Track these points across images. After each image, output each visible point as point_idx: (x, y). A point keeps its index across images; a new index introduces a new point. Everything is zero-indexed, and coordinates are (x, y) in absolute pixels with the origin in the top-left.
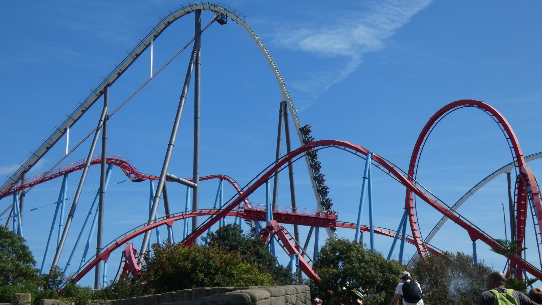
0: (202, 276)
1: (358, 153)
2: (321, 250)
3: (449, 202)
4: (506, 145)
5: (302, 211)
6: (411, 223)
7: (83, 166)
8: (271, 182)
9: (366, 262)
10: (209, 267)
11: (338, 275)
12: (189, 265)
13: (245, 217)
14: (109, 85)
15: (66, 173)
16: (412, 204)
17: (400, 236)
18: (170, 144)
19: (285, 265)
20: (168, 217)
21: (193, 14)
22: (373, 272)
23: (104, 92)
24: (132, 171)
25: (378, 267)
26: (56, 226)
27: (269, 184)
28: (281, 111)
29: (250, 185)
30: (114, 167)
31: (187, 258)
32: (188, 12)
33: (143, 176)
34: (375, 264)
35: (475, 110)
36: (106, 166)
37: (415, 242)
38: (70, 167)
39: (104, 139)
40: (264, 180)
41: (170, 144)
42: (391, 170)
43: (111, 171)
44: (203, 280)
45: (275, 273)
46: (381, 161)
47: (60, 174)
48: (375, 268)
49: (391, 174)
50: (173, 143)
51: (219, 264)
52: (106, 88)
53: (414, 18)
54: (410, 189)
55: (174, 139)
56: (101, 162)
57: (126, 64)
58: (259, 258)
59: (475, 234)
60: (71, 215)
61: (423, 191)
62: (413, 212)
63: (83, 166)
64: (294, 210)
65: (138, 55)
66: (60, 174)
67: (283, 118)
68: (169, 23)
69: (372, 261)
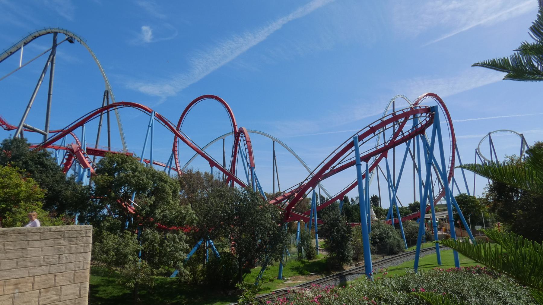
3: (200, 145)
9: (140, 172)
16: (177, 144)
18: (28, 107)
21: (52, 35)
22: (145, 180)
25: (149, 176)
27: (84, 127)
28: (104, 95)
32: (49, 33)
33: (13, 127)
34: (147, 174)
37: (177, 170)
41: (28, 107)
42: (166, 123)
46: (160, 118)
48: (147, 178)
50: (30, 106)
54: (177, 135)
55: (31, 103)
59: (213, 164)
61: (185, 137)
62: (177, 153)
65: (12, 53)
67: (106, 99)
68: (36, 37)
69: (145, 171)
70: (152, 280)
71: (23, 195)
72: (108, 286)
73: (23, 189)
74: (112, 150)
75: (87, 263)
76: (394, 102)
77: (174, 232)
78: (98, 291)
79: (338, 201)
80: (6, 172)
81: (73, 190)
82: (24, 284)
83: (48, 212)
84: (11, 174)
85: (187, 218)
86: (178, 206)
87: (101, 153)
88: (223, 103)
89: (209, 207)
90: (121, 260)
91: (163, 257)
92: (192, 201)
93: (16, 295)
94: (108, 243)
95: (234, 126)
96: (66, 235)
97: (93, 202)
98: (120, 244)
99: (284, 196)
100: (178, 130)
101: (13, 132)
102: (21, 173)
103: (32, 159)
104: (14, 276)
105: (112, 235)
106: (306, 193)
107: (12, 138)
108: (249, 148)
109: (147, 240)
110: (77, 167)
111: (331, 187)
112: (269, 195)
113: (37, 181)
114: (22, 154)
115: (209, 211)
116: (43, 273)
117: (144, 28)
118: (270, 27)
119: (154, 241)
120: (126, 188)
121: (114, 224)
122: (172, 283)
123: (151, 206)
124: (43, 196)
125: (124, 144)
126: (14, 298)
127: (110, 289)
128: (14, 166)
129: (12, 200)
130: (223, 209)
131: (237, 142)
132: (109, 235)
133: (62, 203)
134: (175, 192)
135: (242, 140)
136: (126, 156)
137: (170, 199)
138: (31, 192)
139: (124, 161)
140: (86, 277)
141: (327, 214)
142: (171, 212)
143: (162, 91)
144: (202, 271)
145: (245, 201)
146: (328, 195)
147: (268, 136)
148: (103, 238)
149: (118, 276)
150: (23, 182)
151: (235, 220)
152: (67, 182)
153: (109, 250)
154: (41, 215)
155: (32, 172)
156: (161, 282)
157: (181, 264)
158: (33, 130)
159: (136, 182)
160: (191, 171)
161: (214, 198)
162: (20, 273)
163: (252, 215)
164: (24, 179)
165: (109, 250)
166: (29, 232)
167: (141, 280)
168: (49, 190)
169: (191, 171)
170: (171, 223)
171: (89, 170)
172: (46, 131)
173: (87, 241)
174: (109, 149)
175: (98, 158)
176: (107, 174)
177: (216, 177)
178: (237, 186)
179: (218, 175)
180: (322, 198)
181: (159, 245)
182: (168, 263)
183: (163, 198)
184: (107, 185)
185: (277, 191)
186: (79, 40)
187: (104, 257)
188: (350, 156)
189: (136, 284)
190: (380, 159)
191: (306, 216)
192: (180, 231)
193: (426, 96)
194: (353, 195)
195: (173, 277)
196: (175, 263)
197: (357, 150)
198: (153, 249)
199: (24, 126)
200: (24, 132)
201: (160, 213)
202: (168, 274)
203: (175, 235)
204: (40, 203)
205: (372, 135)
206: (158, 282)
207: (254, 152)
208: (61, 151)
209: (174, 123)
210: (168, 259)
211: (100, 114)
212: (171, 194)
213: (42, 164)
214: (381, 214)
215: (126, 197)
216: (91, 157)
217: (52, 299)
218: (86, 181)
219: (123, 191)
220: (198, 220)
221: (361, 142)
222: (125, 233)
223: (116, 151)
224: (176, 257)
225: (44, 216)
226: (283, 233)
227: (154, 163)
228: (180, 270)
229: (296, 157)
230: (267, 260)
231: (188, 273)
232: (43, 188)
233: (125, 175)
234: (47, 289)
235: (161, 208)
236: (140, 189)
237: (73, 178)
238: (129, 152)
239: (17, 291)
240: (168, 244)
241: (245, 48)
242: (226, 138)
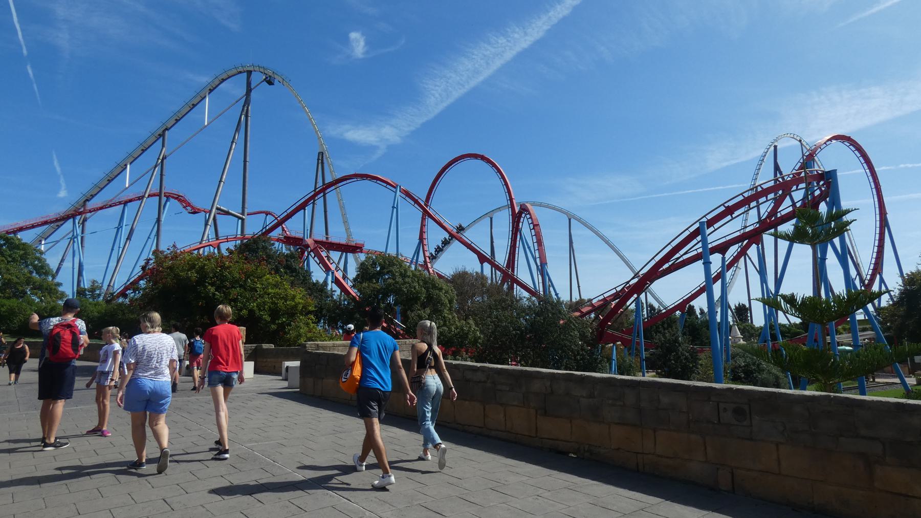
0: (212, 289)
4: (502, 190)
5: (333, 239)
6: (424, 251)
7: (141, 198)
8: (308, 209)
10: (223, 279)
11: (379, 291)
12: (193, 275)
13: (283, 242)
14: (167, 129)
15: (126, 203)
18: (220, 181)
19: (321, 281)
20: (217, 239)
23: (162, 135)
24: (189, 204)
26: (116, 247)
30: (172, 200)
31: (192, 267)
32: (241, 72)
35: (479, 162)
36: (164, 199)
38: (129, 198)
39: (162, 175)
40: (302, 207)
41: (220, 181)
43: (168, 203)
44: (214, 294)
45: (310, 289)
46: (407, 194)
51: (238, 276)
52: (164, 131)
54: (426, 214)
56: (159, 195)
57: (149, 143)
58: (292, 272)
59: (482, 259)
60: (129, 238)
62: (425, 242)
63: (141, 198)
64: (327, 238)
65: (194, 106)
66: (120, 203)
74: (330, 240)
76: (775, 147)
79: (678, 313)
88: (494, 165)
95: (511, 199)
99: (592, 305)
106: (628, 303)
111: (668, 292)
117: (354, 35)
118: (551, 14)
125: (347, 229)
141: (660, 332)
146: (660, 303)
158: (227, 213)
172: (243, 214)
178: (518, 291)
180: (651, 307)
188: (695, 247)
190: (748, 246)
191: (626, 337)
193: (830, 140)
194: (700, 303)
197: (704, 241)
199: (217, 209)
200: (218, 216)
205: (729, 217)
207: (546, 242)
209: (422, 196)
214: (752, 335)
221: (712, 229)
229: (602, 238)
238: (359, 242)
241: (509, 55)
242: (496, 216)
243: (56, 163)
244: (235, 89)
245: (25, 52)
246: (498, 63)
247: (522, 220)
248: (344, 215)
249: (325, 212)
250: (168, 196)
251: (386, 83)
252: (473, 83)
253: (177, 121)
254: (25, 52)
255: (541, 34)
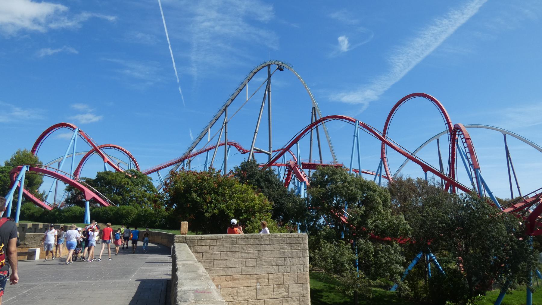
0: (195, 195)
1: (350, 122)
2: (313, 175)
3: (410, 150)
7: (215, 147)
9: (349, 183)
17: (378, 174)
21: (267, 68)
23: (225, 110)
24: (241, 148)
25: (358, 186)
29: (287, 146)
30: (232, 146)
32: (264, 66)
34: (356, 184)
36: (227, 146)
37: (387, 178)
39: (225, 132)
41: (255, 132)
42: (371, 131)
46: (365, 126)
47: (205, 151)
49: (371, 133)
52: (226, 107)
53: (393, 86)
54: (384, 142)
56: (225, 144)
59: (426, 168)
61: (392, 143)
62: (386, 160)
63: (215, 147)
65: (241, 90)
66: (205, 151)
67: (314, 116)
68: (255, 73)
69: (353, 181)
70: (370, 290)
71: (257, 207)
72: (330, 292)
73: (257, 202)
74: (324, 163)
75: (306, 267)
77: (389, 243)
78: (322, 296)
80: (245, 189)
81: (293, 202)
82: (263, 280)
83: (276, 222)
84: (248, 190)
85: (401, 229)
86: (389, 216)
87: (314, 166)
88: (433, 99)
89: (425, 217)
90: (339, 268)
91: (379, 268)
92: (404, 210)
93: (258, 287)
94: (325, 251)
95: (449, 123)
96: (288, 241)
97: (310, 212)
98: (336, 253)
99: (525, 201)
100: (384, 136)
101: (246, 155)
102: (254, 189)
103: (262, 177)
104: (255, 272)
105: (329, 244)
107: (246, 161)
108: (470, 147)
109: (361, 250)
110: (296, 181)
112: (505, 201)
113: (266, 196)
114: (254, 174)
115: (425, 221)
116: (275, 272)
117: (340, 39)
119: (368, 251)
120: (338, 199)
121: (329, 233)
122: (392, 296)
123: (362, 216)
124: (271, 208)
125: (334, 156)
126: (257, 289)
127: (332, 295)
128: (249, 184)
129: (250, 212)
130: (441, 218)
131: (453, 141)
132: (326, 243)
133: (287, 213)
134: (385, 201)
135: (459, 138)
136: (335, 168)
137: (381, 208)
138: (262, 204)
139: (334, 173)
140: (306, 279)
142: (383, 223)
143: (363, 98)
144: (425, 288)
145: (467, 210)
147: (496, 129)
148: (321, 246)
149: (338, 284)
150: (256, 197)
151: (458, 232)
152: (288, 195)
153: (327, 258)
154: (271, 224)
155: (262, 188)
156: (379, 294)
157: (398, 277)
158: (261, 152)
159: (346, 192)
160: (401, 178)
161: (429, 206)
162: (259, 270)
163: (479, 225)
164: (257, 194)
165: (327, 258)
166: (262, 238)
167: (359, 290)
168: (275, 203)
169: (401, 178)
170: (383, 233)
171: (305, 183)
172: (270, 151)
173: (304, 247)
174: (321, 162)
175: (313, 171)
176: (319, 186)
177: (430, 183)
179: (435, 180)
181: (373, 256)
182: (384, 275)
183: (373, 208)
184: (321, 197)
185: (516, 195)
186: (287, 67)
187: (323, 264)
189: (355, 293)
192: (394, 242)
195: (393, 290)
196: (392, 276)
198: (368, 259)
199: (254, 149)
200: (254, 154)
201: (372, 223)
202: (387, 287)
203: (389, 246)
204: (269, 214)
206: (377, 294)
207: (476, 149)
208: (283, 168)
209: (379, 129)
210: (384, 270)
211: (309, 130)
212: (381, 203)
213: (268, 180)
215: (338, 208)
216: (306, 171)
217: (283, 294)
218: (304, 194)
219: (335, 202)
220: (413, 231)
222: (340, 242)
223: (327, 163)
224: (392, 270)
225: (274, 225)
226: (526, 250)
227: (363, 172)
228: (398, 284)
230: (507, 282)
231: (407, 287)
232: (271, 201)
233: (335, 186)
234: (279, 286)
235: (372, 218)
236: (351, 199)
237: (292, 191)
238: (340, 163)
239: (258, 284)
240: (383, 255)
241: (451, 30)
243: (191, 134)
244: (261, 78)
245: (178, 81)
246: (444, 37)
247: (457, 137)
248: (331, 147)
249: (319, 145)
250: (230, 144)
251: (367, 63)
252: (426, 53)
253: (232, 100)
254: (178, 81)
255: (475, 11)
